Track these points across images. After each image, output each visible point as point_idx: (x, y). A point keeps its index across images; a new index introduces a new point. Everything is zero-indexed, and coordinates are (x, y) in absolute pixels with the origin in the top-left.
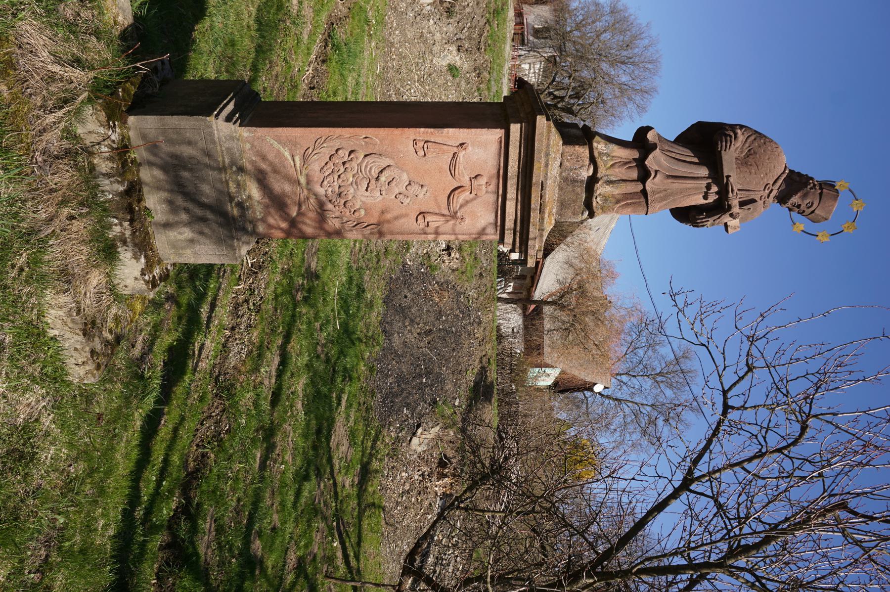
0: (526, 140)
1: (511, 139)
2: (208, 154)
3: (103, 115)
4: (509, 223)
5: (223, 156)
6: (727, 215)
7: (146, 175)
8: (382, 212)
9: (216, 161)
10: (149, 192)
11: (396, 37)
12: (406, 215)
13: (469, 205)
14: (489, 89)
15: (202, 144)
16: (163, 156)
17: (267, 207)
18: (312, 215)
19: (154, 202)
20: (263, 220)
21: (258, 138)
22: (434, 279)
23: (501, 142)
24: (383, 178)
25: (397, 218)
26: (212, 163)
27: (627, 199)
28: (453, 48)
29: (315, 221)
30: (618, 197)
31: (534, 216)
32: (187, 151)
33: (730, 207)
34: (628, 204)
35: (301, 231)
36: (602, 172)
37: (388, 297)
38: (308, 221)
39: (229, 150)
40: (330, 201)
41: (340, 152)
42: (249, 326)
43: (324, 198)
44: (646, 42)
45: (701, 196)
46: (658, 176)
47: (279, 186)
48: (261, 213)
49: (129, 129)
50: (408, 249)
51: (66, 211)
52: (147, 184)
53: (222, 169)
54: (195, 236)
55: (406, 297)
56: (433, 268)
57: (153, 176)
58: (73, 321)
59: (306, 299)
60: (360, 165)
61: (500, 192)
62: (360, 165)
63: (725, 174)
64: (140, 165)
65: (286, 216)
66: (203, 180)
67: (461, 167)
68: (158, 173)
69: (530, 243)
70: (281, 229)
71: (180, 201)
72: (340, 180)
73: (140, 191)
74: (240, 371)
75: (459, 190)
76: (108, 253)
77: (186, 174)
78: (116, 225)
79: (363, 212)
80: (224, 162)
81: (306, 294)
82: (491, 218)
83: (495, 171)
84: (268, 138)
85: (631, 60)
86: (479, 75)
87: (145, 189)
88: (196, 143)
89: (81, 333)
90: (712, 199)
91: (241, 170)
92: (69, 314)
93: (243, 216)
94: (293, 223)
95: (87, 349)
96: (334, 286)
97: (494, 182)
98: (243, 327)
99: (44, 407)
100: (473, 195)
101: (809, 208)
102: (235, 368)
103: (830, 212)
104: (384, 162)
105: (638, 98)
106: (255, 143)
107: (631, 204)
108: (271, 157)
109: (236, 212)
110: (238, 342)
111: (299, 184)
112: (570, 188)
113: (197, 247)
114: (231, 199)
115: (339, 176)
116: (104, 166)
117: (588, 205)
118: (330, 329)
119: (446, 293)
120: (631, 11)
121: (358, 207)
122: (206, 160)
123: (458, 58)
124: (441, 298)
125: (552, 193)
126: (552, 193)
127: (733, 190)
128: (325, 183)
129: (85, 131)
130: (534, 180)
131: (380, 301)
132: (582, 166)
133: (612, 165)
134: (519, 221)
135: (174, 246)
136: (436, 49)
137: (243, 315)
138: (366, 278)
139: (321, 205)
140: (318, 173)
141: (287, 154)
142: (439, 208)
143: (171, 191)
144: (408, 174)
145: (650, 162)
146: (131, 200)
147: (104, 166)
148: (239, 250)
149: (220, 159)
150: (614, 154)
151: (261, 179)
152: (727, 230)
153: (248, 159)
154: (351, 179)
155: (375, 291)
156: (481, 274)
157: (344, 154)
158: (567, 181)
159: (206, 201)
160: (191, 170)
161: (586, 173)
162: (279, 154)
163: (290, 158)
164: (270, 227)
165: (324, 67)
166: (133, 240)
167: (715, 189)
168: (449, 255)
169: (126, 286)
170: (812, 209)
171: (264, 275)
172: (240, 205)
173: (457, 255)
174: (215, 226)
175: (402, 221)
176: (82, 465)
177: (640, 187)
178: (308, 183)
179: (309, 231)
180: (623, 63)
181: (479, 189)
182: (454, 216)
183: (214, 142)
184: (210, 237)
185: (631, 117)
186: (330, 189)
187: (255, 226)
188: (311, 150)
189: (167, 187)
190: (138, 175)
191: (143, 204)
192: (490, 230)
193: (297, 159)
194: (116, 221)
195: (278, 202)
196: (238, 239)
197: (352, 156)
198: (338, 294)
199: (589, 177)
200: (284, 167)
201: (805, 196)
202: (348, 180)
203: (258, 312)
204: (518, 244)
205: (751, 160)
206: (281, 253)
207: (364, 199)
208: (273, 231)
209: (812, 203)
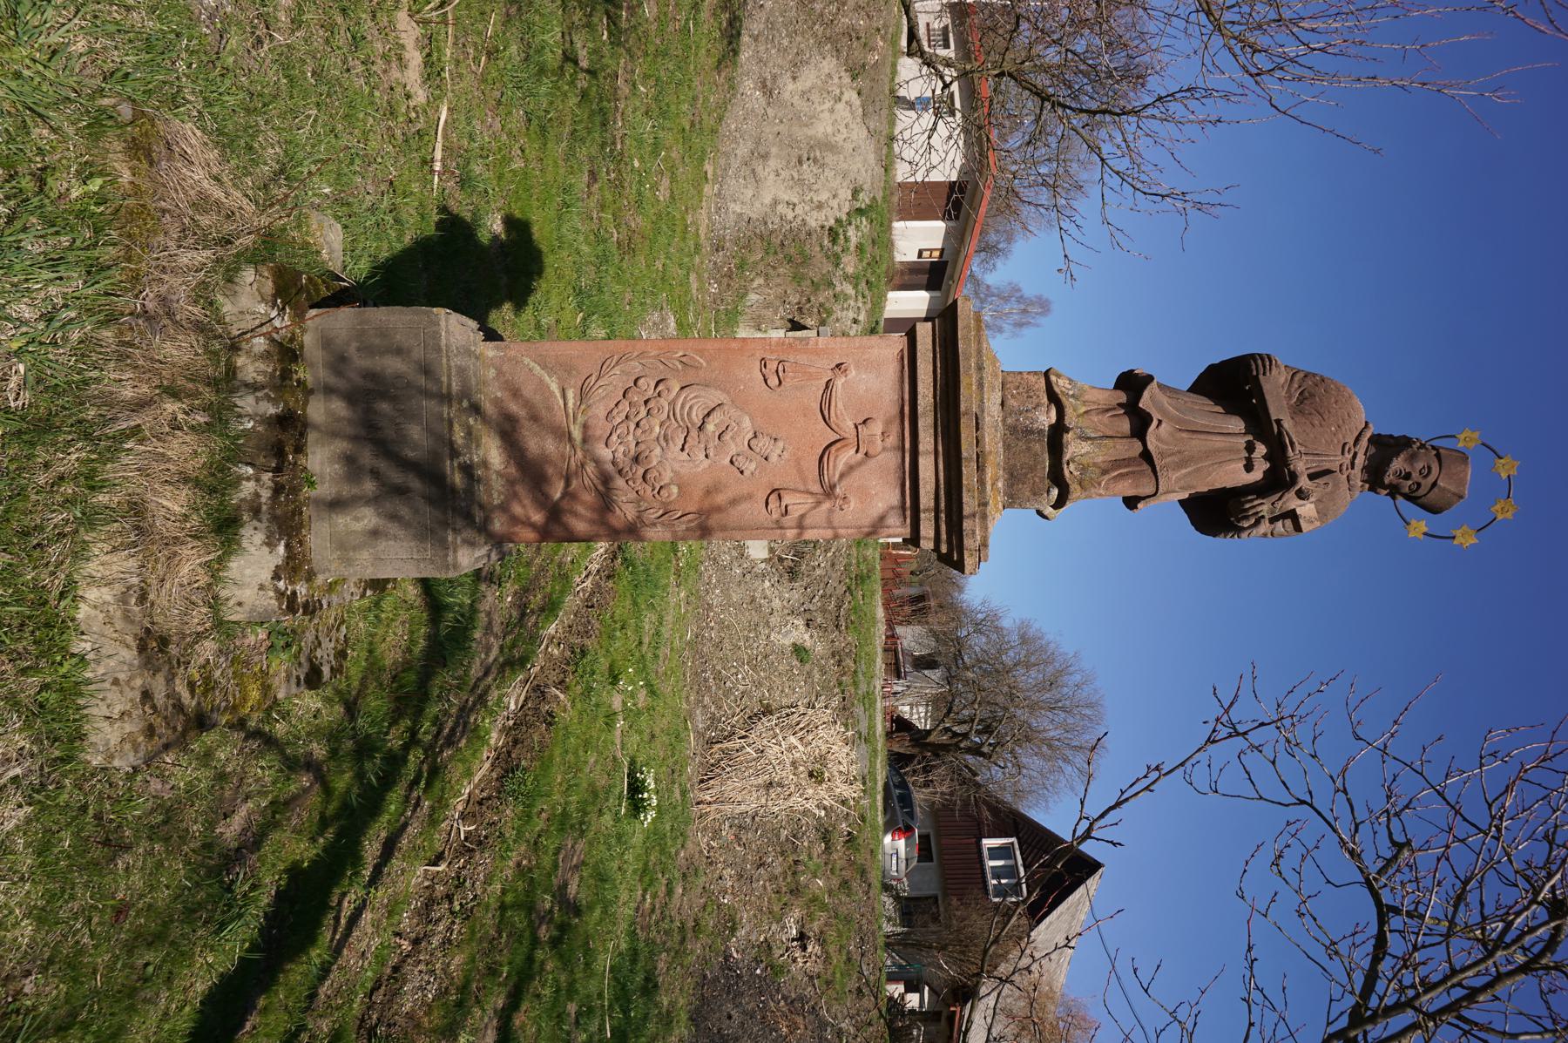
2: (427, 370)
3: (269, 287)
4: (926, 500)
5: (449, 376)
6: (1292, 493)
7: (317, 410)
8: (708, 492)
9: (438, 381)
10: (317, 441)
11: (716, 598)
12: (750, 497)
13: (856, 474)
14: (855, 684)
15: (418, 353)
16: (353, 375)
17: (511, 483)
18: (588, 497)
19: (321, 461)
20: (504, 508)
21: (510, 359)
22: (778, 991)
24: (710, 427)
25: (734, 502)
26: (430, 386)
28: (800, 622)
29: (594, 510)
32: (392, 365)
33: (1294, 477)
35: (566, 528)
36: (1070, 419)
37: (698, 1010)
38: (580, 509)
39: (462, 371)
40: (620, 472)
41: (641, 382)
42: (447, 942)
43: (610, 467)
44: (1077, 678)
45: (1241, 465)
47: (537, 443)
48: (500, 493)
49: (304, 331)
50: (733, 930)
51: (171, 406)
52: (316, 427)
53: (446, 398)
54: (381, 522)
55: (730, 1017)
56: (777, 970)
57: (329, 413)
58: (127, 617)
59: (555, 943)
60: (672, 403)
61: (907, 445)
62: (672, 403)
63: (1274, 418)
64: (311, 392)
65: (542, 500)
66: (413, 416)
67: (840, 405)
68: (339, 406)
69: (966, 524)
70: (533, 526)
71: (367, 457)
72: (639, 431)
73: (302, 435)
74: (418, 1026)
75: (838, 445)
76: (224, 528)
77: (384, 407)
78: (248, 479)
79: (675, 490)
80: (449, 385)
81: (555, 933)
82: (894, 498)
83: (895, 411)
84: (527, 360)
86: (839, 663)
87: (312, 436)
88: (409, 351)
89: (134, 644)
90: (1257, 475)
91: (476, 409)
92: (123, 599)
93: (470, 492)
94: (555, 513)
95: (138, 682)
96: (606, 950)
97: (895, 429)
98: (436, 941)
99: (15, 779)
100: (860, 455)
102: (410, 1016)
103: (1462, 482)
104: (716, 396)
106: (505, 368)
108: (528, 391)
109: (458, 479)
110: (422, 967)
111: (570, 439)
113: (382, 545)
114: (454, 453)
115: (638, 425)
116: (251, 368)
117: (1057, 477)
118: (594, 1027)
119: (799, 1020)
120: (1049, 637)
121: (666, 480)
122: (422, 381)
123: (807, 637)
124: (793, 1027)
125: (993, 440)
126: (993, 440)
127: (1292, 443)
128: (614, 437)
129: (235, 310)
130: (963, 408)
131: (684, 1016)
132: (1038, 405)
134: (942, 492)
135: (343, 545)
136: (773, 620)
137: (439, 920)
138: (661, 965)
139: (606, 479)
140: (602, 421)
141: (554, 387)
142: (804, 480)
143: (354, 439)
144: (752, 419)
145: (1145, 403)
146: (286, 434)
147: (251, 369)
148: (455, 551)
149: (444, 379)
151: (508, 432)
153: (491, 394)
154: (657, 429)
155: (676, 995)
156: (859, 990)
157: (647, 384)
158: (1017, 433)
159: (411, 454)
160: (394, 399)
161: (1046, 418)
162: (542, 387)
163: (558, 394)
164: (515, 520)
165: (610, 584)
166: (272, 508)
167: (1261, 449)
168: (804, 948)
169: (240, 604)
170: (1431, 479)
171: (484, 859)
172: (467, 470)
173: (818, 949)
174: (420, 503)
175: (744, 506)
176: (56, 989)
178: (585, 440)
179: (580, 526)
181: (871, 442)
182: (829, 492)
183: (439, 350)
184: (405, 525)
186: (621, 449)
187: (487, 520)
188: (593, 378)
189: (349, 430)
190: (304, 410)
191: (302, 461)
192: (894, 520)
193: (570, 394)
194: (250, 471)
195: (531, 473)
196: (454, 530)
197: (660, 388)
198: (611, 971)
199: (1051, 427)
200: (549, 409)
201: (1412, 458)
202: (651, 429)
203: (468, 918)
204: (944, 536)
205: (1307, 408)
206: (520, 834)
207: (677, 466)
208: (517, 529)
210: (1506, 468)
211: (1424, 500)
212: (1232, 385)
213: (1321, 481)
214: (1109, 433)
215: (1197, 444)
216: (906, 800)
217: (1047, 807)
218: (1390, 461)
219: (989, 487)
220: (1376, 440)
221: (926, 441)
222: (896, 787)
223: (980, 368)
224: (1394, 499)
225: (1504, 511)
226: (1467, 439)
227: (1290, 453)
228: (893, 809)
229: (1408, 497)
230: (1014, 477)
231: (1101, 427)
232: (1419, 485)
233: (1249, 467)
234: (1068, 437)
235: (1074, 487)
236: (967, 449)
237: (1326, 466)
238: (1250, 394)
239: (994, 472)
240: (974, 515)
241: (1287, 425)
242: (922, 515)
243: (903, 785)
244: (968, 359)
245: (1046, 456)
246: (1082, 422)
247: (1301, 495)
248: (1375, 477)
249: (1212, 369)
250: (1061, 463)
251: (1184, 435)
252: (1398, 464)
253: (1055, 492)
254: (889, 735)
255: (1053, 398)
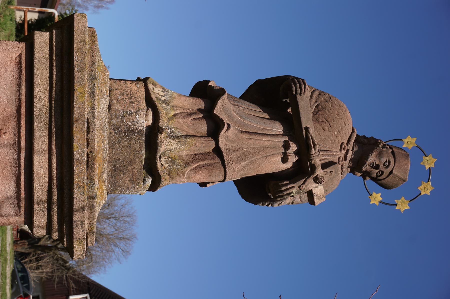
0: (60, 56)
1: (37, 55)
4: (40, 192)
6: (311, 180)
23: (20, 63)
27: (198, 160)
30: (186, 158)
31: (80, 172)
33: (314, 168)
34: (200, 167)
36: (164, 123)
45: (279, 158)
46: (232, 128)
61: (23, 144)
63: (304, 126)
69: (76, 217)
83: (11, 110)
85: (113, 216)
90: (289, 165)
101: (387, 167)
105: (122, 244)
107: (204, 166)
112: (124, 142)
127: (315, 145)
130: (76, 114)
132: (139, 110)
133: (175, 116)
134: (55, 187)
150: (175, 103)
152: (312, 201)
158: (121, 132)
161: (145, 121)
167: (294, 147)
170: (390, 169)
177: (212, 144)
180: (108, 218)
185: (119, 260)
199: (148, 127)
201: (380, 155)
204: (55, 225)
209: (389, 162)
210: (429, 162)
211: (383, 181)
212: (274, 96)
213: (328, 170)
214: (192, 133)
215: (253, 143)
216: (25, 279)
217: (105, 270)
218: (367, 157)
219: (96, 181)
220: (360, 140)
221: (41, 141)
222: (19, 271)
223: (93, 78)
224: (365, 179)
225: (426, 189)
226: (409, 143)
227: (313, 152)
228: (18, 285)
229: (373, 179)
230: (116, 169)
231: (186, 128)
232: (383, 172)
233: (285, 160)
234: (162, 137)
235: (165, 177)
236: (79, 151)
237: (331, 159)
238: (288, 105)
239: (102, 169)
240: (83, 209)
241: (312, 131)
242: (36, 207)
243: (24, 270)
244: (82, 70)
245: (144, 152)
246: (173, 124)
247: (317, 180)
248: (357, 165)
249: (259, 83)
250: (155, 158)
251: (245, 136)
252: (372, 159)
253: (149, 181)
254: (15, 242)
255: (151, 103)
